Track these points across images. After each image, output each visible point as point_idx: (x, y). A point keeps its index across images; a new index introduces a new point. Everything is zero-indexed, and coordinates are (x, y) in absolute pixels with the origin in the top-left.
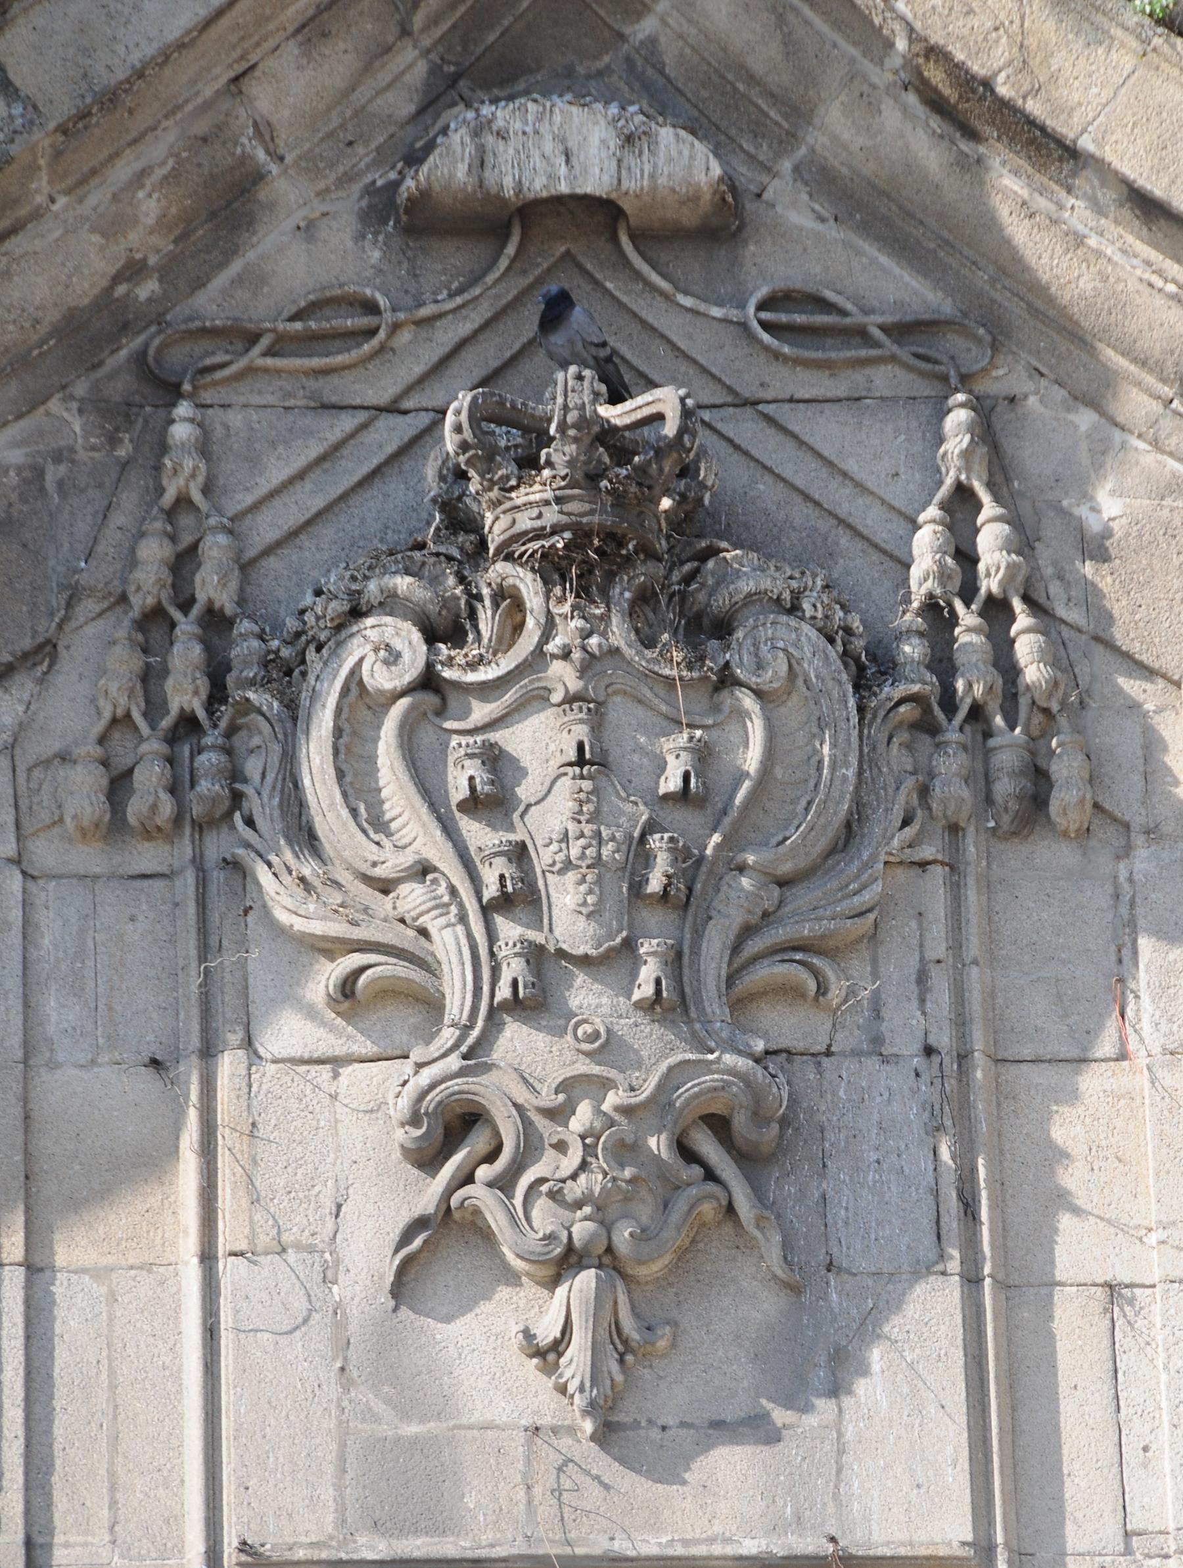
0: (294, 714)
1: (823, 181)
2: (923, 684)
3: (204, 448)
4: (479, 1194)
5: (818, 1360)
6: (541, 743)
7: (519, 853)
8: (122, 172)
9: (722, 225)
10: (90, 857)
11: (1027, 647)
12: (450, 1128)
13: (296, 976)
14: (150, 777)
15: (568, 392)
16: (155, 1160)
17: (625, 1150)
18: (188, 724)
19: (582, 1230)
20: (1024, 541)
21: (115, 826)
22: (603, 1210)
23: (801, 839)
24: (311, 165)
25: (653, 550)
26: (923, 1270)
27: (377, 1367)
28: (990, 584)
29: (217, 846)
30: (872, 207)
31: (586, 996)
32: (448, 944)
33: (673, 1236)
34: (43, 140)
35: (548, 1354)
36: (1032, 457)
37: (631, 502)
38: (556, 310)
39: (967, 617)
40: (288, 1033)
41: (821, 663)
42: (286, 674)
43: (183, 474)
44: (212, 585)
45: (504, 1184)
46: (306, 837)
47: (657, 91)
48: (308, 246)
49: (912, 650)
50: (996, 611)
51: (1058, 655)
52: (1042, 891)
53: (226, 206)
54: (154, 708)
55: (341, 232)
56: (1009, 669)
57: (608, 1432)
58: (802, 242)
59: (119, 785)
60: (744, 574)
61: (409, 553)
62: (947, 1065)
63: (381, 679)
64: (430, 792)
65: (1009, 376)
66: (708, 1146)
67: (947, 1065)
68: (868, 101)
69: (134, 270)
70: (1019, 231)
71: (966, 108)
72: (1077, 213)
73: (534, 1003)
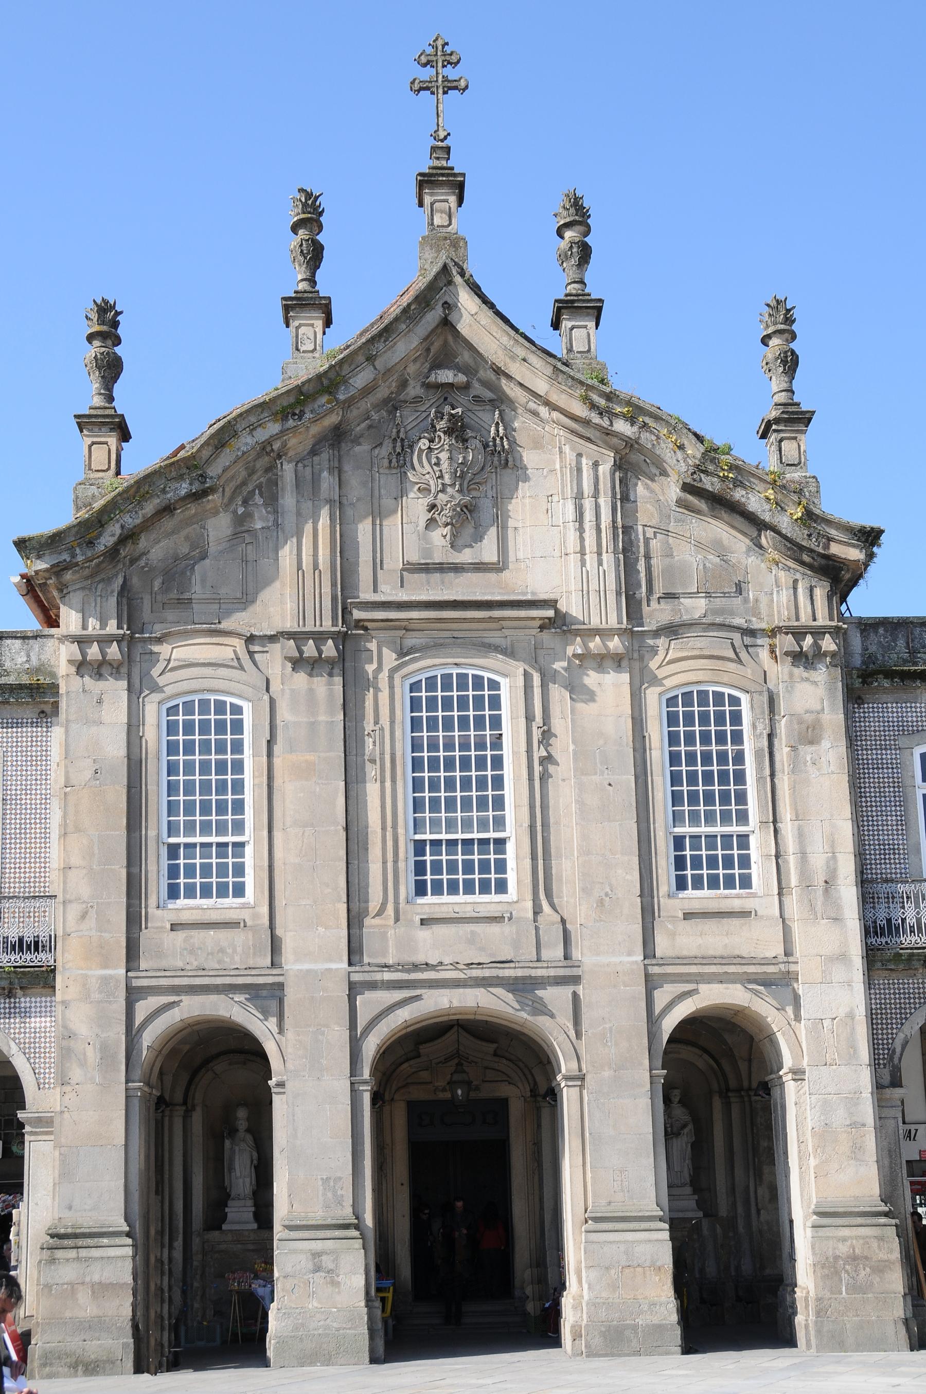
0: (412, 452)
1: (479, 380)
2: (492, 448)
3: (401, 416)
4: (436, 516)
5: (478, 537)
6: (444, 456)
7: (441, 471)
8: (390, 380)
9: (466, 387)
10: (387, 471)
11: (505, 443)
12: (432, 507)
13: (413, 487)
14: (394, 460)
15: (447, 409)
16: (396, 511)
17: (454, 510)
18: (399, 453)
19: (449, 520)
20: (505, 429)
21: (390, 467)
22: (452, 518)
23: (476, 469)
24: (414, 379)
25: (458, 430)
26: (492, 526)
27: (424, 538)
28: (501, 435)
29: (403, 470)
30: (486, 384)
31: (449, 489)
32: (432, 483)
33: (460, 521)
34: (380, 375)
35: (445, 536)
36: (506, 418)
37: (455, 424)
38: (446, 399)
39: (498, 439)
40: (411, 495)
41: (479, 445)
42: (411, 447)
43: (398, 420)
44: (402, 435)
45: (439, 514)
46: (414, 469)
47: (459, 369)
48: (414, 390)
49: (491, 444)
50: (502, 438)
51: (509, 444)
52: (507, 476)
53: (404, 384)
54: (395, 451)
55: (418, 388)
56: (503, 446)
57: (452, 547)
58: (478, 389)
59: (390, 462)
60: (470, 433)
61: (426, 431)
62: (495, 499)
63: (423, 447)
64: (430, 463)
65: (503, 407)
66: (465, 510)
67: (495, 499)
68: (485, 370)
69: (392, 393)
70: (505, 387)
71: (498, 371)
72: (512, 385)
73: (443, 491)
